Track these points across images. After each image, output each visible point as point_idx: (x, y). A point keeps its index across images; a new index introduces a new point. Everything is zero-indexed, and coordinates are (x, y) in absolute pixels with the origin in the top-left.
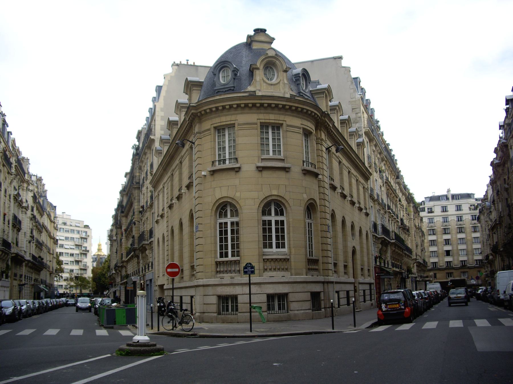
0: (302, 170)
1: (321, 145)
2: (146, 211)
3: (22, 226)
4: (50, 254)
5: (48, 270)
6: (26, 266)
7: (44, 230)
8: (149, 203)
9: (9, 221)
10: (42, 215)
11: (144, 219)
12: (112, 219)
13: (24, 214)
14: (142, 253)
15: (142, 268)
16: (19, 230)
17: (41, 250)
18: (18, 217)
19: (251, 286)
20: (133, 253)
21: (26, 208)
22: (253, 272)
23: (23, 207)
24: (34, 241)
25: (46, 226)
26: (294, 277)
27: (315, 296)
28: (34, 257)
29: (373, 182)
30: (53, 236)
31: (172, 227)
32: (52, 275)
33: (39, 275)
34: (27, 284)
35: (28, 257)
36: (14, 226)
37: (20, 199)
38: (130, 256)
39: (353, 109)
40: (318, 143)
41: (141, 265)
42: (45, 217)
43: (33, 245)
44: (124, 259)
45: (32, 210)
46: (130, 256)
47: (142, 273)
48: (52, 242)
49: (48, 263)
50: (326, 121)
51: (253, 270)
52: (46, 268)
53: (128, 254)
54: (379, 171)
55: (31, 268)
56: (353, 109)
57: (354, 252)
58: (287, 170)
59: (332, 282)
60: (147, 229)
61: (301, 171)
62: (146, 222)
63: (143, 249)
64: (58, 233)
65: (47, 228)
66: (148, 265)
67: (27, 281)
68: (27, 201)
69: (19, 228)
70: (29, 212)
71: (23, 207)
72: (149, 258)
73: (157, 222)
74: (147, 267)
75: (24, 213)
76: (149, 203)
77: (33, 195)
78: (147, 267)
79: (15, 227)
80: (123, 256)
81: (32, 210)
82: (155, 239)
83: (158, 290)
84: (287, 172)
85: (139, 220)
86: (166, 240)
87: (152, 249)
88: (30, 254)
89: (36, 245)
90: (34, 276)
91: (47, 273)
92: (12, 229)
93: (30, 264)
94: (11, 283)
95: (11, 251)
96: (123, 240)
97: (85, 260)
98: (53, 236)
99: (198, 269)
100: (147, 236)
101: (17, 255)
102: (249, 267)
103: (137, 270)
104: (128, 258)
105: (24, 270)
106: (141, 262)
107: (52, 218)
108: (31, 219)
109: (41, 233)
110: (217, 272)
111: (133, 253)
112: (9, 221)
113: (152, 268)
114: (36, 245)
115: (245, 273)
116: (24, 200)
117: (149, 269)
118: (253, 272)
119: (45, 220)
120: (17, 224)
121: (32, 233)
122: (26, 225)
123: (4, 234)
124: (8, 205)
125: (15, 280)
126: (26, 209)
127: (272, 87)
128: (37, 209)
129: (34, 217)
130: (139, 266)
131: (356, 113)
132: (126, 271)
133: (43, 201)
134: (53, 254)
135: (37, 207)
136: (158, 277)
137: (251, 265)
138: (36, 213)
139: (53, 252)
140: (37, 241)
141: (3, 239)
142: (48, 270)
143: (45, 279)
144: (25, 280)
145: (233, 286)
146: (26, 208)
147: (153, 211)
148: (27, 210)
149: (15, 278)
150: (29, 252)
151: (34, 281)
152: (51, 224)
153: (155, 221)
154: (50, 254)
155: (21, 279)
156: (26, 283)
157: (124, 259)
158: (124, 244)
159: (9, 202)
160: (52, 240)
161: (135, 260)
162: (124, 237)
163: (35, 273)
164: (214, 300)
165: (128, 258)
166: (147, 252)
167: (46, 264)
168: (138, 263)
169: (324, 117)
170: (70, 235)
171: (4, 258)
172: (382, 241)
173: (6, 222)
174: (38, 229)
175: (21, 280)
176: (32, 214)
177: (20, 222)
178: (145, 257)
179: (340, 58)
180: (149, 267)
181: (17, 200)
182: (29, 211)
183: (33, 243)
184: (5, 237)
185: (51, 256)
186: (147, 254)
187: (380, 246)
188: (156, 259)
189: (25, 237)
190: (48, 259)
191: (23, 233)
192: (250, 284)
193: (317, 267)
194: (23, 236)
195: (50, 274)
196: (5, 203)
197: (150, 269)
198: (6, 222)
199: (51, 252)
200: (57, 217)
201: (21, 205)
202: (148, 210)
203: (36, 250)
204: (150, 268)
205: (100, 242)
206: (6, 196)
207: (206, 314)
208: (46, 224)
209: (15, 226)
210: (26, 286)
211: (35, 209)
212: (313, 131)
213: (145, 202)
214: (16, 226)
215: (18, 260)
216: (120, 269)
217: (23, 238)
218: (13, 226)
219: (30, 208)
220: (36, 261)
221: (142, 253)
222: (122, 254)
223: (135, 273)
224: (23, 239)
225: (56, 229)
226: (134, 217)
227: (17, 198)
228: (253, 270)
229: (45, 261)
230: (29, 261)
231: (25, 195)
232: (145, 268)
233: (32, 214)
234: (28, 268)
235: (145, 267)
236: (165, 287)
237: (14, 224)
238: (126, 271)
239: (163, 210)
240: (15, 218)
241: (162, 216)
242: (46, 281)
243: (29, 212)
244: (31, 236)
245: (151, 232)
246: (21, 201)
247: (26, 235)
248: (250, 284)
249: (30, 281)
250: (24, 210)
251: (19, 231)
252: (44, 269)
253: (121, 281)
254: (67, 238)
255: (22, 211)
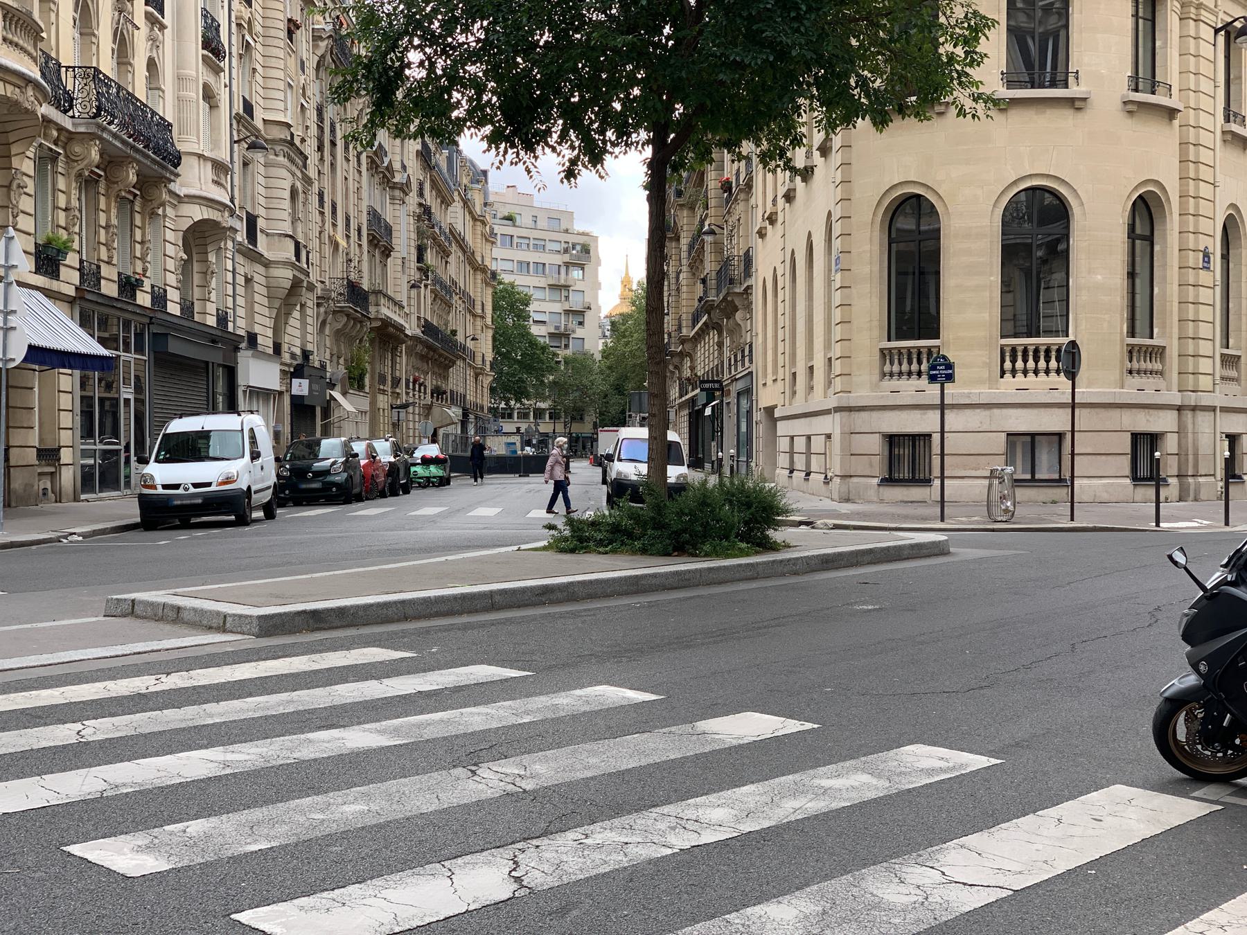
0: (1125, 103)
1: (1195, 21)
2: (736, 200)
4: (475, 316)
5: (470, 366)
6: (410, 352)
7: (454, 248)
8: (742, 176)
9: (359, 230)
10: (446, 202)
11: (732, 220)
12: (601, 255)
13: (397, 207)
14: (728, 318)
15: (730, 360)
16: (387, 252)
17: (450, 306)
18: (383, 217)
19: (1077, 411)
20: (706, 316)
21: (404, 188)
22: (950, 378)
23: (394, 187)
24: (429, 282)
25: (460, 235)
26: (1083, 392)
28: (428, 328)
30: (483, 262)
31: (793, 251)
32: (480, 377)
33: (446, 378)
34: (414, 404)
35: (412, 329)
36: (374, 242)
37: (385, 164)
38: (700, 325)
40: (1187, 16)
41: (727, 353)
42: (457, 206)
43: (426, 294)
44: (685, 331)
45: (421, 194)
46: (700, 325)
47: (730, 373)
48: (479, 281)
49: (470, 344)
51: (951, 371)
52: (464, 359)
53: (695, 320)
55: (423, 358)
58: (1078, 104)
60: (739, 252)
61: (1119, 105)
62: (736, 230)
63: (729, 309)
64: (498, 252)
65: (463, 240)
66: (743, 351)
67: (414, 395)
68: (404, 167)
69: (386, 248)
70: (413, 199)
71: (394, 187)
72: (744, 332)
73: (762, 234)
74: (739, 357)
75: (398, 202)
76: (742, 176)
77: (419, 147)
78: (739, 357)
79: (376, 246)
80: (684, 323)
81: (421, 194)
82: (756, 282)
83: (763, 421)
84: (1079, 109)
86: (780, 286)
87: (748, 307)
88: (419, 318)
90: (430, 381)
91: (468, 372)
92: (369, 252)
93: (419, 348)
94: (373, 403)
95: (368, 312)
96: (681, 276)
98: (483, 262)
100: (737, 272)
101: (386, 323)
102: (940, 365)
103: (717, 365)
104: (697, 328)
105: (404, 365)
106: (727, 342)
107: (478, 209)
108: (419, 218)
109: (448, 256)
110: (884, 375)
111: (706, 316)
112: (359, 230)
113: (751, 361)
114: (432, 291)
115: (933, 379)
116: (397, 166)
117: (743, 365)
118: (950, 378)
121: (420, 259)
122: (404, 239)
123: (348, 266)
124: (356, 185)
126: (402, 189)
128: (434, 185)
129: (427, 211)
130: (721, 353)
132: (692, 368)
133: (450, 159)
134: (483, 317)
136: (765, 385)
137: (946, 360)
138: (430, 198)
139: (483, 310)
140: (437, 281)
141: (349, 282)
142: (470, 366)
143: (461, 390)
144: (407, 394)
145: (922, 412)
146: (404, 188)
147: (752, 201)
148: (407, 195)
149: (382, 387)
150: (416, 315)
151: (432, 397)
152: (474, 225)
153: (756, 230)
154: (475, 316)
155: (398, 390)
156: (411, 400)
158: (684, 289)
159: (357, 175)
160: (479, 276)
161: (713, 336)
162: (685, 268)
163: (433, 373)
164: (875, 445)
165: (697, 328)
166: (739, 316)
167: (465, 346)
168: (720, 345)
170: (532, 257)
171: (354, 334)
173: (353, 234)
174: (439, 246)
175: (398, 394)
176: (420, 205)
177: (389, 230)
178: (736, 330)
180: (743, 356)
181: (377, 166)
182: (411, 194)
183: (426, 286)
184: (353, 276)
185: (479, 322)
186: (740, 322)
188: (760, 336)
189: (404, 272)
191: (399, 262)
192: (942, 407)
193: (1157, 366)
194: (400, 268)
195: (477, 375)
196: (346, 178)
197: (747, 364)
198: (353, 234)
200: (491, 205)
201: (389, 181)
202: (742, 196)
203: (436, 308)
204: (747, 359)
205: (627, 274)
206: (348, 160)
207: (855, 480)
208: (459, 227)
209: (376, 242)
210: (411, 409)
211: (427, 186)
213: (734, 172)
214: (379, 241)
215: (388, 336)
217: (399, 275)
218: (370, 242)
219: (415, 186)
220: (437, 339)
221: (728, 318)
222: (680, 319)
223: (712, 372)
225: (490, 238)
226: (707, 214)
227: (379, 162)
228: (951, 371)
229: (460, 338)
230: (415, 338)
231: (398, 150)
232: (736, 361)
233: (420, 205)
234: (413, 359)
235: (736, 356)
236: (777, 414)
237: (374, 237)
238: (692, 368)
239: (774, 201)
240: (374, 216)
242: (465, 396)
243: (413, 199)
244: (419, 269)
245: (748, 260)
246: (390, 168)
247: (407, 265)
248: (942, 407)
249: (420, 397)
250: (397, 193)
251: (388, 256)
253: (681, 396)
254: (524, 266)
255: (393, 198)
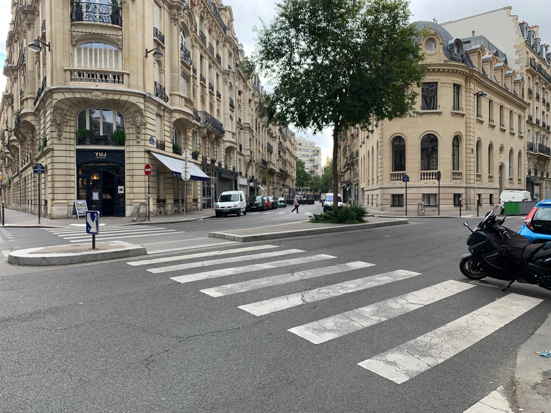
3: (273, 150)
4: (292, 167)
7: (287, 151)
10: (285, 141)
11: (354, 143)
16: (271, 153)
17: (286, 165)
21: (275, 138)
22: (408, 180)
23: (273, 137)
27: (457, 196)
28: (281, 170)
29: (533, 110)
33: (285, 182)
35: (277, 170)
36: (268, 150)
39: (517, 52)
41: (352, 175)
42: (288, 142)
43: (281, 162)
44: (342, 170)
45: (279, 139)
49: (291, 174)
50: (474, 75)
53: (344, 167)
54: (542, 101)
55: (280, 177)
56: (517, 52)
57: (501, 167)
59: (474, 188)
61: (450, 114)
63: (353, 164)
64: (298, 152)
68: (275, 133)
70: (277, 140)
71: (273, 137)
73: (361, 146)
81: (279, 139)
85: (350, 144)
87: (358, 164)
89: (283, 163)
93: (279, 175)
94: (268, 188)
97: (317, 171)
99: (275, 190)
100: (355, 155)
105: (275, 179)
106: (352, 173)
107: (293, 142)
115: (404, 181)
116: (274, 132)
118: (408, 180)
119: (287, 144)
120: (270, 150)
121: (279, 154)
125: (271, 185)
126: (275, 138)
127: (431, 56)
130: (351, 175)
131: (519, 55)
132: (344, 179)
133: (286, 131)
135: (282, 136)
138: (281, 140)
140: (283, 159)
146: (275, 138)
154: (292, 167)
157: (342, 170)
160: (293, 158)
162: (342, 155)
164: (389, 197)
166: (355, 166)
168: (351, 173)
169: (473, 73)
170: (305, 153)
172: (538, 157)
173: (264, 148)
177: (272, 147)
178: (354, 170)
179: (510, 8)
185: (293, 169)
187: (536, 161)
190: (291, 171)
192: (406, 188)
195: (292, 181)
198: (264, 148)
199: (293, 166)
202: (356, 137)
208: (288, 147)
211: (281, 137)
212: (462, 84)
215: (272, 172)
216: (340, 177)
218: (268, 150)
219: (278, 137)
224: (274, 158)
225: (295, 149)
229: (288, 172)
230: (278, 173)
238: (344, 179)
239: (364, 138)
240: (269, 145)
241: (363, 143)
243: (277, 140)
245: (357, 153)
246: (272, 133)
248: (406, 188)
250: (274, 139)
252: (288, 178)
254: (304, 155)
